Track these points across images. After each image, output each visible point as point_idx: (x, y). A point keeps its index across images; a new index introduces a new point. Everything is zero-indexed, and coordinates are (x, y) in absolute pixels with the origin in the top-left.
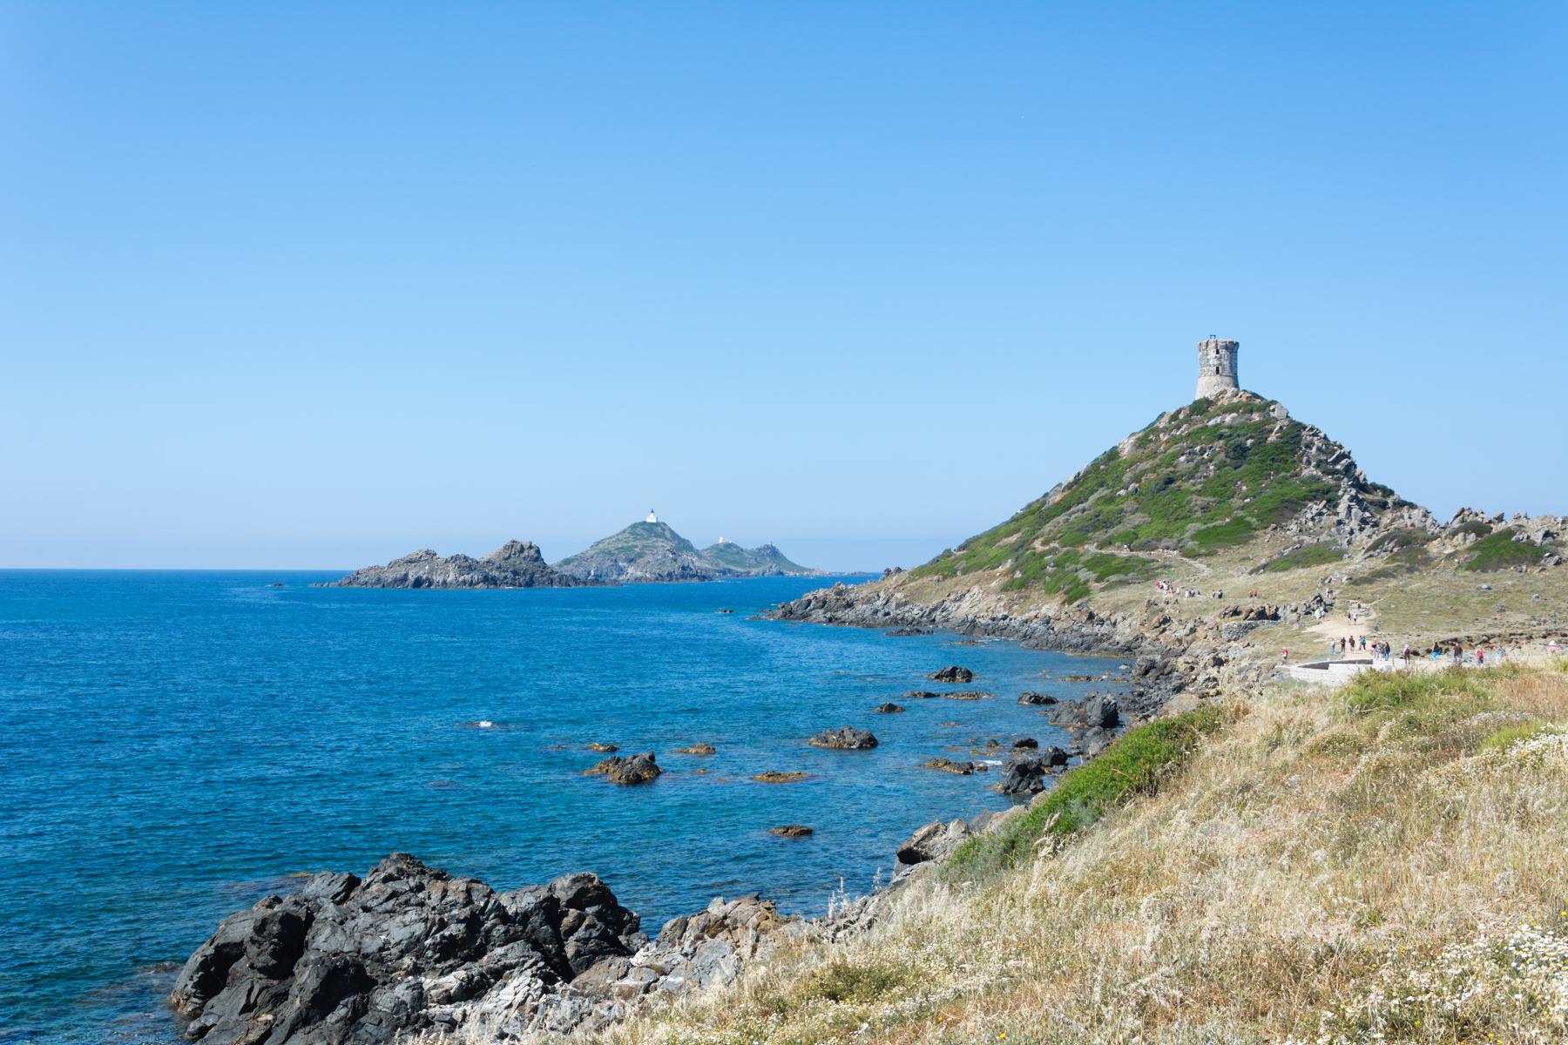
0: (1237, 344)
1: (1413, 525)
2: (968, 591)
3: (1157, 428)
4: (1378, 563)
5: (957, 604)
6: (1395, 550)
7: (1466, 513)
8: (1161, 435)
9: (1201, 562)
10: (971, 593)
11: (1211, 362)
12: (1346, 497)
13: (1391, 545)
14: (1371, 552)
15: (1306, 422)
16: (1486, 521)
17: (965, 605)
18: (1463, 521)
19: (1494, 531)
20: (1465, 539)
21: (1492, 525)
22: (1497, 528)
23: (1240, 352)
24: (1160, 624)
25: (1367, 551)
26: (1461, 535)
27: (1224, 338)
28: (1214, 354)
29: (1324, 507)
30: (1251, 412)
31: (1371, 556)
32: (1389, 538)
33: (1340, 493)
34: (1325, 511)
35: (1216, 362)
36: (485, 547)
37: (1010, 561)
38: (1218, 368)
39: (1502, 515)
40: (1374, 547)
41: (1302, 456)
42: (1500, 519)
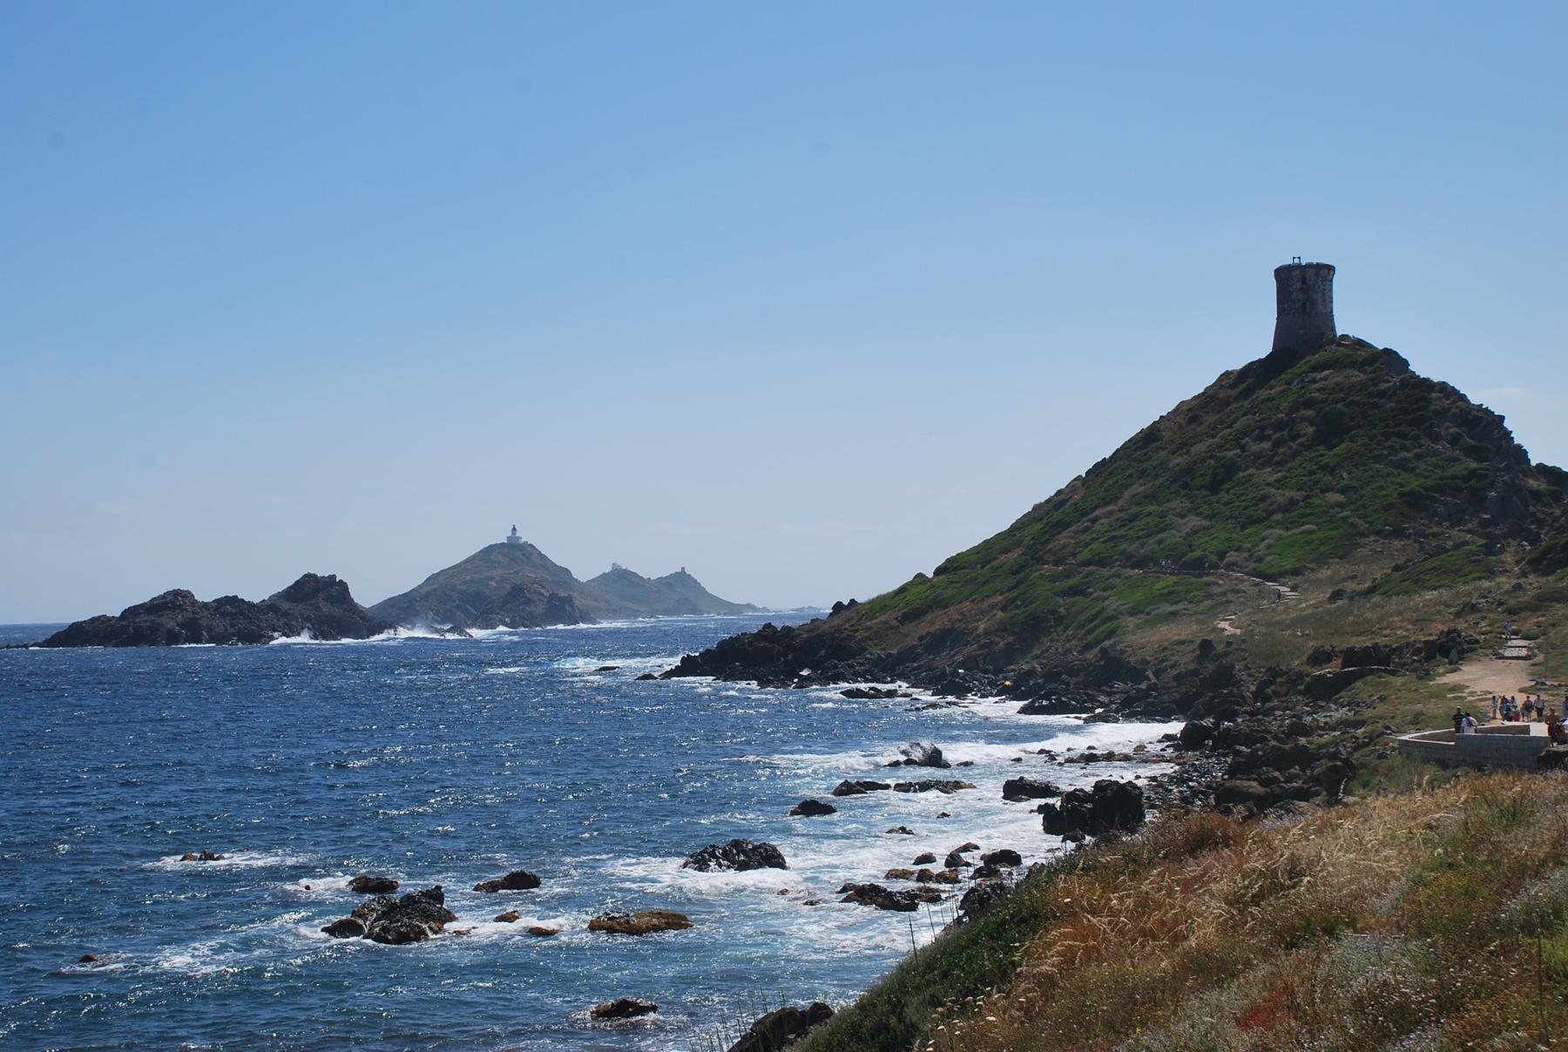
11: (1294, 295)
28: (1298, 285)
35: (1301, 296)
38: (1304, 305)
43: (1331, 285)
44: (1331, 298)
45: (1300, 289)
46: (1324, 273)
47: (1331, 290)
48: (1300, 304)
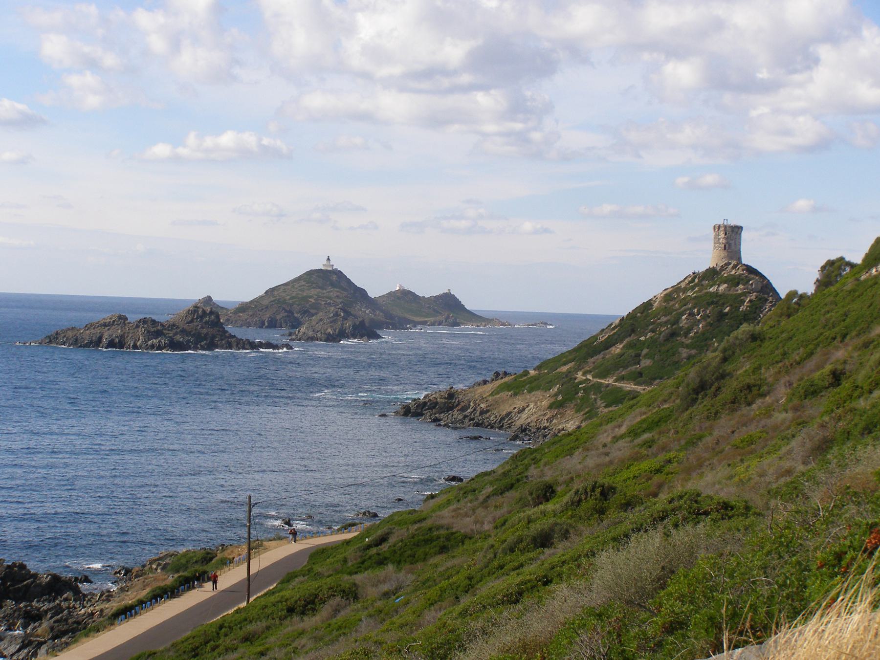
8: (681, 294)
11: (721, 241)
23: (744, 235)
27: (733, 222)
30: (738, 284)
38: (725, 245)
45: (724, 238)
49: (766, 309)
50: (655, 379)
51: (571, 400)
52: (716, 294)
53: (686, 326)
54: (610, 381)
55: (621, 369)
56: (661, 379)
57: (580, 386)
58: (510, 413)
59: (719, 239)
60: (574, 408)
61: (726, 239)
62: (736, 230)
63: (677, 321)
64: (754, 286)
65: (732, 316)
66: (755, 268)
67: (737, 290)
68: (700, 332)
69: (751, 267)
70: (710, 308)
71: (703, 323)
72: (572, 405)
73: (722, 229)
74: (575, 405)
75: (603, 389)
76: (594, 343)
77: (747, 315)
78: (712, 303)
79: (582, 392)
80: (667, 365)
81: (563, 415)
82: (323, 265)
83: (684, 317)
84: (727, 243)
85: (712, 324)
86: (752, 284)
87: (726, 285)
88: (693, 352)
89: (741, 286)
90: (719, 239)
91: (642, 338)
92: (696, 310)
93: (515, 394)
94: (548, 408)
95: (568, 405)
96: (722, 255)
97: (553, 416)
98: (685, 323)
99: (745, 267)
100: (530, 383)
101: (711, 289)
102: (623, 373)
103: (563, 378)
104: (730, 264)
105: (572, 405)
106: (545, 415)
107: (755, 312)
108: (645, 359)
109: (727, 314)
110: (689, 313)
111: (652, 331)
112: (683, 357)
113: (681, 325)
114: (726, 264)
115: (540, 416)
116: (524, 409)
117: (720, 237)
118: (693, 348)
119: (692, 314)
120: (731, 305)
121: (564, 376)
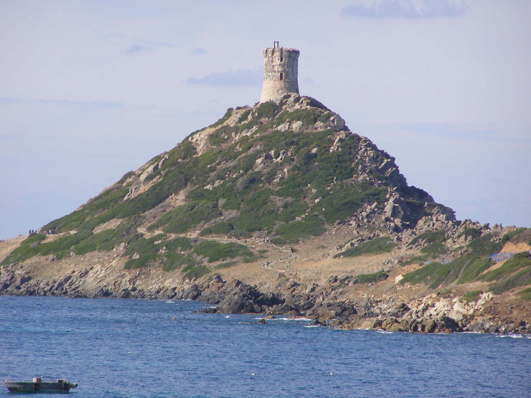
0: (297, 53)
1: (436, 229)
2: (91, 269)
3: (227, 126)
4: (416, 252)
5: (83, 279)
6: (426, 245)
7: (468, 223)
8: (233, 134)
9: (286, 249)
10: (94, 270)
11: (276, 68)
12: (391, 200)
13: (423, 242)
14: (411, 246)
15: (361, 134)
16: (479, 228)
17: (90, 279)
18: (466, 228)
19: (380, 236)
20: (466, 239)
21: (482, 231)
22: (485, 232)
23: (301, 60)
24: (292, 286)
25: (409, 245)
26: (463, 237)
27: (288, 46)
28: (279, 62)
29: (376, 207)
30: (315, 121)
31: (411, 248)
32: (422, 237)
33: (388, 196)
34: (376, 209)
36: (525, 227)
37: (123, 244)
38: (281, 74)
39: (488, 224)
40: (413, 242)
41: (357, 165)
42: (487, 227)
43: (297, 62)
44: (297, 70)
45: (280, 64)
46: (297, 53)
47: (297, 66)
48: (279, 74)
49: (361, 149)
50: (253, 230)
51: (154, 257)
52: (289, 133)
53: (265, 171)
54: (193, 235)
55: (202, 222)
56: (260, 230)
57: (156, 243)
58: (70, 277)
59: (273, 66)
60: (160, 267)
61: (283, 66)
62: (293, 55)
63: (250, 165)
64: (335, 123)
65: (323, 157)
66: (320, 101)
67: (317, 128)
68: (286, 177)
69: (315, 100)
70: (291, 150)
71: (288, 167)
72: (157, 264)
73: (277, 54)
74: (161, 263)
75: (192, 244)
76: (123, 196)
77: (341, 156)
78: (292, 143)
79: (165, 248)
80: (261, 214)
81: (147, 275)
82: (282, 48)
83: (259, 161)
84: (284, 71)
85: (299, 168)
86: (333, 121)
87: (300, 123)
88: (289, 199)
89: (319, 124)
90: (273, 66)
91: (209, 187)
92: (272, 152)
93: (59, 258)
94: (125, 268)
95: (151, 264)
96: (278, 86)
97: (136, 277)
98: (263, 168)
99: (309, 101)
100: (75, 244)
101: (279, 128)
102: (206, 226)
103: (124, 236)
104: (289, 96)
105: (157, 264)
106: (123, 276)
107: (350, 153)
108: (227, 210)
109: (315, 155)
110: (266, 155)
111: (221, 177)
112: (278, 206)
113: (256, 170)
114: (285, 97)
115: (118, 277)
116: (87, 272)
117: (274, 64)
118: (288, 195)
119: (268, 157)
120: (318, 146)
121: (124, 233)
